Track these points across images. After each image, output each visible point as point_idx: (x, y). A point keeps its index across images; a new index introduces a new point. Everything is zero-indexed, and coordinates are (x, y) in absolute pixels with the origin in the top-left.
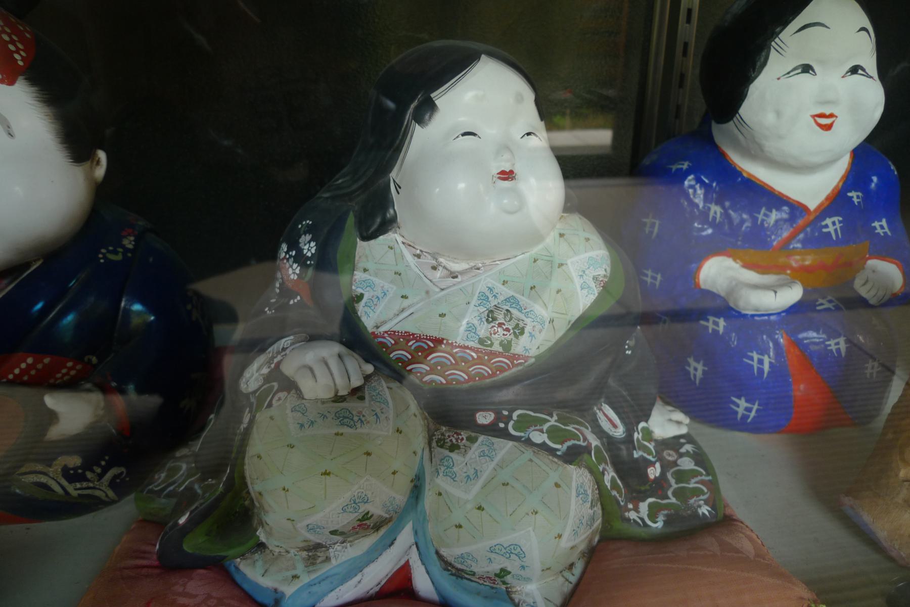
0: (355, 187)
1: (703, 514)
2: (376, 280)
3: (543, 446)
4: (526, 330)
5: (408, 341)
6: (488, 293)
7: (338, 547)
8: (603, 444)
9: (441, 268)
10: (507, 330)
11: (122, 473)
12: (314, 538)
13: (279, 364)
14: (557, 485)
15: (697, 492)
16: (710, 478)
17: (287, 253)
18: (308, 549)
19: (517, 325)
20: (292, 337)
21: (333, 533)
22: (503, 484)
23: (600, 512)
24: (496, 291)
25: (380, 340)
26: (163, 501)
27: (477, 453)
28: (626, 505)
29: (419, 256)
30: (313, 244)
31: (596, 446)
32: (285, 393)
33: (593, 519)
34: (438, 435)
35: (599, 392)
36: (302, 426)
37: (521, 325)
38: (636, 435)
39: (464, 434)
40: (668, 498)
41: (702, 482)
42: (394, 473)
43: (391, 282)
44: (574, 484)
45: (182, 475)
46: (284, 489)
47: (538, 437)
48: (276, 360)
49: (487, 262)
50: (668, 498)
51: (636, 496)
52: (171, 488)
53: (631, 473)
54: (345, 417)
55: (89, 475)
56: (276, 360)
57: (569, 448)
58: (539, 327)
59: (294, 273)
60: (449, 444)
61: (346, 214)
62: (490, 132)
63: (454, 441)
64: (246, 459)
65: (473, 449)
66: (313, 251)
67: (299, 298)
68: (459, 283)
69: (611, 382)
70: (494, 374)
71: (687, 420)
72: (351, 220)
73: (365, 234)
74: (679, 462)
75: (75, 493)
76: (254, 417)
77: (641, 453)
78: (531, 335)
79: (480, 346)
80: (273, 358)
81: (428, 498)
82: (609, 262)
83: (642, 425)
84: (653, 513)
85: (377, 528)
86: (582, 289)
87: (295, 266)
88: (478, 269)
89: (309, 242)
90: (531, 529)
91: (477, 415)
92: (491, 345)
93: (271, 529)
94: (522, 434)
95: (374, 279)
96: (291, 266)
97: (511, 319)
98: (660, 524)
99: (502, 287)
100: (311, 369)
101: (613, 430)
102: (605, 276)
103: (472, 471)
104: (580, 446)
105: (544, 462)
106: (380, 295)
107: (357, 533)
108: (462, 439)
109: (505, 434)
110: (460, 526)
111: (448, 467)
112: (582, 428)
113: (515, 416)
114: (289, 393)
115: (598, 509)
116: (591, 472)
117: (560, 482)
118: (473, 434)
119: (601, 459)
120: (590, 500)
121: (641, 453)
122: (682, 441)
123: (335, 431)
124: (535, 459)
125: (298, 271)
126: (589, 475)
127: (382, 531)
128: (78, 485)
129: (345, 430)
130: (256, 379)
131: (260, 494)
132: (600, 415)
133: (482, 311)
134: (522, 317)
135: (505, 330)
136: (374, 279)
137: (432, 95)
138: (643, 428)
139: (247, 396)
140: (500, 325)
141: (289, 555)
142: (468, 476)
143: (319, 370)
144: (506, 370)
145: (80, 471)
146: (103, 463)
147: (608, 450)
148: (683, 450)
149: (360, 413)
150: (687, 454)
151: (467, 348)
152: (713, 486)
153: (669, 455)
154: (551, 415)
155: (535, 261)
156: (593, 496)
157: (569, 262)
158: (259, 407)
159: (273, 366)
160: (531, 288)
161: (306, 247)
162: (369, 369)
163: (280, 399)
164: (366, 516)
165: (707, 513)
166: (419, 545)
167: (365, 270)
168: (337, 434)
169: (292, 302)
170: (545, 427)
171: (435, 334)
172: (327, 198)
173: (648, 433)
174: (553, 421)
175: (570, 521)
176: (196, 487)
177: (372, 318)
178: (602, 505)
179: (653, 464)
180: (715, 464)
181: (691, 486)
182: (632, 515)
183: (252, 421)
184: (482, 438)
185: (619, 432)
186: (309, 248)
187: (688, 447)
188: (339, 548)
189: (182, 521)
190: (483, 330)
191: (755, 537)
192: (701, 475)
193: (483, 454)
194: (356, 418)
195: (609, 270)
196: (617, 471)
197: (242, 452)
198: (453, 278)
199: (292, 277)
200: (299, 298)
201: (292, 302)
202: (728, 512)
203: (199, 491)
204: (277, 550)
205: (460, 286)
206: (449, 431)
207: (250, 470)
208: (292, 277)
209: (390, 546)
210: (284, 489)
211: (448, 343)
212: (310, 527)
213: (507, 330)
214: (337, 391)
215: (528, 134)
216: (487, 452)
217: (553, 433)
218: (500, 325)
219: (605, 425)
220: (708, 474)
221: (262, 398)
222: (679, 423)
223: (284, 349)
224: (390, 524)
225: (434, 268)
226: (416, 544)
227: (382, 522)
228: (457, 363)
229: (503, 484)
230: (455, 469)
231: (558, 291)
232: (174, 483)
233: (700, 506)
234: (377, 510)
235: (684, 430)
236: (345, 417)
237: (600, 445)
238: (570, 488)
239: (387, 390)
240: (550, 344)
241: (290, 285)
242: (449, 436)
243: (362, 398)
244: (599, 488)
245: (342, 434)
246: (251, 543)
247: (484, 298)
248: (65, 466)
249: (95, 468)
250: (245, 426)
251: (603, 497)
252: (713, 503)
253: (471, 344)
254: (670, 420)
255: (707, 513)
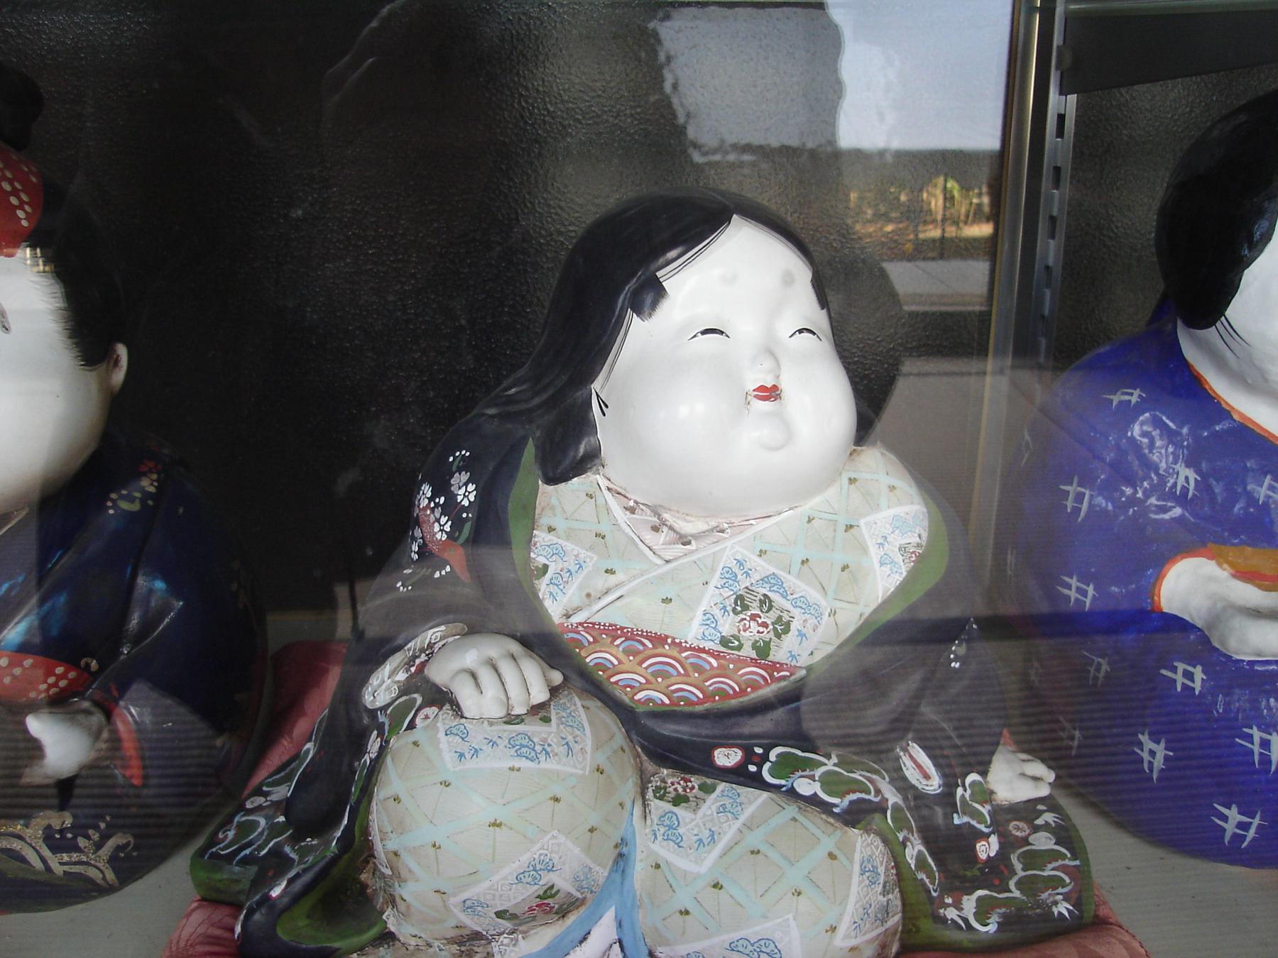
0: (536, 401)
1: (1060, 913)
2: (569, 546)
3: (813, 800)
4: (794, 626)
5: (615, 638)
6: (736, 570)
7: (504, 939)
8: (905, 799)
9: (665, 529)
10: (765, 625)
11: (128, 844)
12: (473, 924)
13: (424, 664)
14: (832, 856)
15: (1054, 882)
16: (1077, 863)
17: (430, 499)
18: (459, 941)
19: (780, 618)
20: (443, 628)
21: (500, 914)
22: (752, 852)
23: (899, 903)
24: (748, 566)
25: (571, 635)
26: (237, 869)
27: (714, 808)
28: (941, 897)
29: (632, 510)
30: (471, 487)
31: (896, 808)
32: (435, 709)
33: (886, 910)
34: (655, 781)
35: (904, 725)
36: (461, 755)
37: (786, 618)
38: (960, 791)
39: (695, 781)
40: (1010, 891)
41: (1063, 868)
42: (591, 830)
43: (591, 548)
44: (857, 857)
45: (261, 833)
46: (434, 846)
47: (805, 787)
48: (418, 661)
49: (736, 521)
50: (1010, 891)
51: (958, 885)
52: (247, 852)
53: (951, 848)
54: (522, 746)
55: (82, 842)
56: (418, 661)
57: (851, 802)
58: (813, 621)
59: (442, 531)
60: (673, 795)
61: (524, 440)
62: (745, 329)
63: (680, 790)
64: (374, 803)
65: (709, 802)
66: (472, 498)
67: (448, 569)
68: (692, 552)
69: (928, 711)
70: (743, 692)
71: (1051, 776)
72: (529, 452)
73: (551, 475)
74: (1031, 839)
75: (58, 870)
76: (387, 742)
77: (966, 819)
78: (801, 635)
79: (723, 649)
80: (415, 657)
81: (639, 870)
82: (926, 523)
83: (973, 777)
84: (983, 912)
85: (563, 913)
86: (882, 564)
87: (444, 519)
88: (722, 531)
89: (466, 484)
90: (790, 916)
91: (716, 753)
92: (740, 648)
93: (408, 907)
94: (783, 782)
95: (564, 543)
96: (438, 520)
97: (770, 608)
98: (992, 928)
99: (758, 559)
100: (474, 675)
101: (924, 782)
102: (918, 545)
103: (707, 833)
104: (870, 801)
105: (813, 823)
106: (574, 569)
107: (534, 918)
108: (693, 788)
109: (756, 782)
110: (687, 913)
111: (670, 827)
112: (874, 777)
113: (773, 755)
114: (440, 709)
115: (895, 898)
116: (885, 841)
117: (836, 852)
118: (709, 781)
119: (900, 822)
120: (882, 881)
121: (966, 819)
122: (1040, 807)
123: (511, 765)
124: (800, 818)
125: (447, 528)
126: (881, 846)
127: (572, 918)
128: (66, 857)
129: (523, 763)
130: (388, 688)
131: (396, 854)
132: (905, 759)
133: (726, 595)
134: (787, 605)
135: (759, 625)
136: (564, 543)
137: (659, 274)
138: (973, 784)
139: (373, 713)
140: (754, 617)
141: (431, 950)
142: (700, 840)
143: (486, 676)
144: (760, 687)
145: (69, 836)
146: (103, 825)
147: (915, 809)
148: (1039, 822)
149: (544, 740)
150: (1046, 827)
151: (703, 650)
152: (1081, 875)
153: (1018, 828)
154: (828, 757)
155: (809, 521)
156: (887, 876)
157: (862, 522)
158: (395, 727)
159: (413, 669)
160: (803, 562)
161: (462, 491)
162: (557, 677)
163: (427, 717)
164: (550, 892)
165: (1066, 914)
166: (625, 944)
167: (551, 529)
168: (512, 769)
169: (437, 575)
170: (818, 772)
171: (656, 629)
172: (493, 416)
173: (986, 795)
174: (830, 765)
175: (850, 908)
176: (287, 849)
177: (558, 603)
178: (901, 891)
179: (987, 836)
180: (1090, 844)
181: (1045, 874)
182: (951, 914)
183: (383, 750)
184: (722, 786)
185: (934, 785)
186: (466, 493)
187: (1049, 817)
188: (506, 941)
189: (276, 892)
190: (728, 625)
191: (1136, 945)
192: (1063, 857)
193: (723, 809)
194: (538, 748)
195: (925, 535)
196: (927, 842)
197: (367, 792)
198: (684, 544)
199: (438, 536)
200: (448, 569)
201: (437, 575)
202: (1103, 912)
203: (293, 855)
204: (413, 942)
205: (695, 557)
206: (673, 776)
207: (379, 818)
208: (438, 536)
209: (581, 942)
210: (434, 846)
211: (673, 642)
212: (469, 903)
213: (765, 625)
214: (509, 707)
215: (801, 331)
216: (729, 806)
217: (829, 782)
218: (754, 617)
219: (912, 774)
220: (1074, 857)
221: (401, 717)
222: (1036, 779)
223: (431, 645)
224: (582, 910)
225: (656, 529)
226: (620, 942)
227: (573, 903)
228: (687, 674)
229: (752, 852)
230: (681, 830)
231: (844, 568)
232: (249, 844)
233: (1056, 903)
234: (563, 883)
235: (1044, 791)
236: (522, 746)
237: (901, 802)
238: (852, 862)
239: (581, 710)
240: (829, 649)
241: (435, 548)
242: (673, 784)
243: (547, 720)
244: (897, 866)
245: (519, 770)
246: (374, 932)
247: (730, 576)
248: (49, 827)
249: (91, 832)
250: (373, 756)
251: (901, 877)
252: (1077, 900)
253: (708, 645)
254: (1023, 775)
255: (1066, 914)
